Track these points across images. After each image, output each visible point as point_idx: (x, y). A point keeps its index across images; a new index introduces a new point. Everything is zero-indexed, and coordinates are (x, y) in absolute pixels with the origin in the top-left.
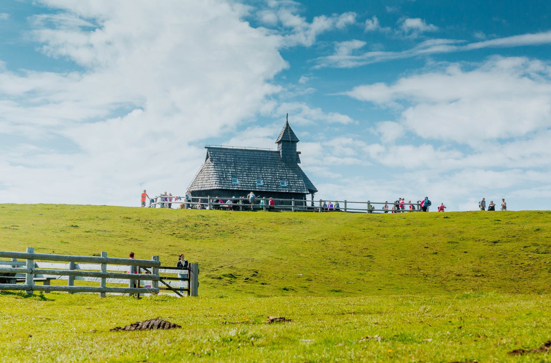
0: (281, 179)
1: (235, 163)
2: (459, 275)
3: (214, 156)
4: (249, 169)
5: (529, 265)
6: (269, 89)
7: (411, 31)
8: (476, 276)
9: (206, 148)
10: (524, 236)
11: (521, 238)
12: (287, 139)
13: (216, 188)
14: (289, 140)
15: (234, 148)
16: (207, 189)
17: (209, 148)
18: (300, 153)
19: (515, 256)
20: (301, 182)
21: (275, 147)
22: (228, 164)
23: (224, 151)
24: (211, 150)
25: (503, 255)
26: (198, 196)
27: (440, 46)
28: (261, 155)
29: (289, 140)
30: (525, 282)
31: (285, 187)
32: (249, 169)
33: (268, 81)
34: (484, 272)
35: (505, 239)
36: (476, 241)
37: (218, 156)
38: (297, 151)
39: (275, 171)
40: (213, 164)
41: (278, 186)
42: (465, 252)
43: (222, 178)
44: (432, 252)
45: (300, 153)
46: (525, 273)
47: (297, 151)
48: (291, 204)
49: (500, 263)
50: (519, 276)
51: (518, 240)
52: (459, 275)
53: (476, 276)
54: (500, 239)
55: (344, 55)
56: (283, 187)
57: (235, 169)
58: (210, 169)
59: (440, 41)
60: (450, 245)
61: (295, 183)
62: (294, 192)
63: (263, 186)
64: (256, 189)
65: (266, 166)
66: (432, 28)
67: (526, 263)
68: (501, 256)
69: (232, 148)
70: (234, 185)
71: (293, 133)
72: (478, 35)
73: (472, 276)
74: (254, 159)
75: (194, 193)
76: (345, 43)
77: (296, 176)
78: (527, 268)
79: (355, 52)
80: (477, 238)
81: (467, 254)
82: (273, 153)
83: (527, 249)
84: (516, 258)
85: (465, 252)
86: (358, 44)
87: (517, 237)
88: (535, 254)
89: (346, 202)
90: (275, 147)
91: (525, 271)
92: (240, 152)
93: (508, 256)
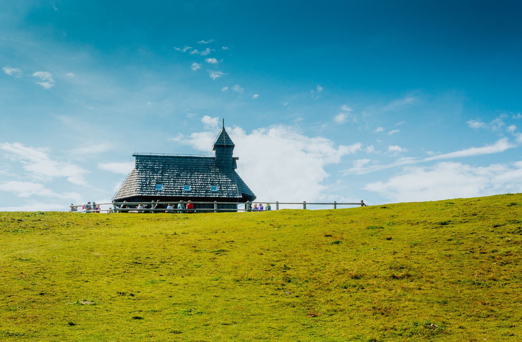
0: (212, 184)
1: (164, 171)
2: (356, 277)
3: (141, 164)
4: (178, 175)
5: (508, 254)
6: (321, 188)
7: (393, 152)
8: (394, 277)
9: (134, 156)
10: (491, 213)
11: (485, 215)
12: (222, 144)
13: (135, 195)
14: (224, 146)
15: (165, 155)
16: (126, 197)
17: (137, 156)
18: (238, 158)
19: (480, 239)
20: (234, 186)
21: (212, 154)
22: (153, 170)
23: (154, 158)
24: (139, 158)
25: (456, 240)
26: (125, 204)
27: (408, 160)
28: (194, 162)
29: (224, 146)
30: (508, 288)
31: (216, 192)
32: (178, 175)
33: (320, 183)
34: (414, 270)
35: (460, 219)
36: (412, 224)
37: (146, 163)
38: (233, 156)
39: (207, 176)
40: (138, 171)
41: (207, 191)
42: (389, 239)
43: (143, 186)
44: (334, 240)
45: (238, 158)
46: (503, 268)
47: (233, 156)
48: (213, 208)
49: (449, 253)
50: (491, 275)
51: (482, 218)
52: (356, 277)
53: (394, 277)
54: (452, 219)
55: (359, 167)
56: (213, 192)
57: (162, 176)
58: (134, 176)
59: (409, 158)
60: (370, 231)
61: (228, 187)
62: (225, 196)
63: (190, 192)
64: (181, 194)
65: (198, 172)
66: (405, 150)
67: (502, 250)
68: (452, 242)
69: (163, 155)
70: (157, 192)
71: (229, 138)
72: (430, 153)
73: (385, 278)
74: (187, 165)
75: (116, 201)
76: (359, 161)
77: (230, 180)
78: (505, 258)
79: (365, 166)
80: (414, 221)
81: (391, 241)
82: (208, 160)
83: (499, 229)
84: (482, 244)
85: (389, 239)
86: (366, 161)
87: (480, 214)
88: (516, 236)
89: (277, 204)
90: (212, 154)
91: (502, 264)
92: (171, 159)
93: (464, 241)
